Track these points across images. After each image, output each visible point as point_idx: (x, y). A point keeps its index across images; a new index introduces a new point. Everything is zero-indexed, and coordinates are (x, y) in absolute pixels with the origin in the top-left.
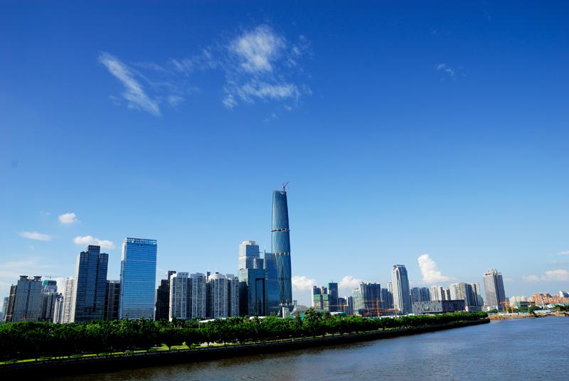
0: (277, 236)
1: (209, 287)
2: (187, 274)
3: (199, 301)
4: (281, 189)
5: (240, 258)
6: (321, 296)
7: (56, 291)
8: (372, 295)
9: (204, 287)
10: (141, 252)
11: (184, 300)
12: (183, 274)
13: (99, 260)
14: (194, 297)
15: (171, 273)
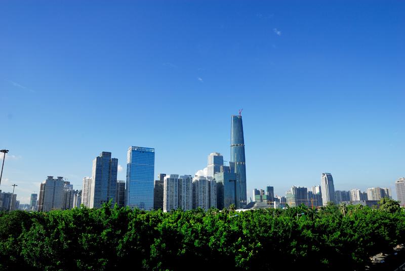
0: (235, 150)
1: (195, 185)
2: (178, 176)
3: (187, 198)
4: (238, 114)
6: (261, 197)
7: (72, 188)
8: (301, 196)
9: (191, 186)
10: (143, 158)
11: (176, 196)
12: (175, 175)
13: (110, 163)
14: (184, 194)
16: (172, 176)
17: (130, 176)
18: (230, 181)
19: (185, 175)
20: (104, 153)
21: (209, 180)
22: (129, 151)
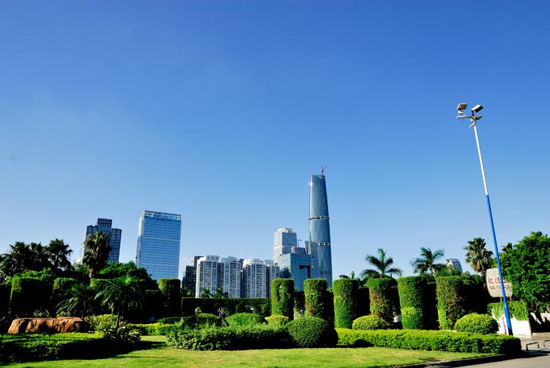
2: (217, 258)
4: (319, 173)
5: (275, 248)
9: (237, 273)
10: (163, 228)
15: (197, 258)
16: (208, 258)
17: (140, 257)
18: (302, 267)
19: (230, 257)
20: (101, 221)
21: (268, 265)
22: (141, 219)
